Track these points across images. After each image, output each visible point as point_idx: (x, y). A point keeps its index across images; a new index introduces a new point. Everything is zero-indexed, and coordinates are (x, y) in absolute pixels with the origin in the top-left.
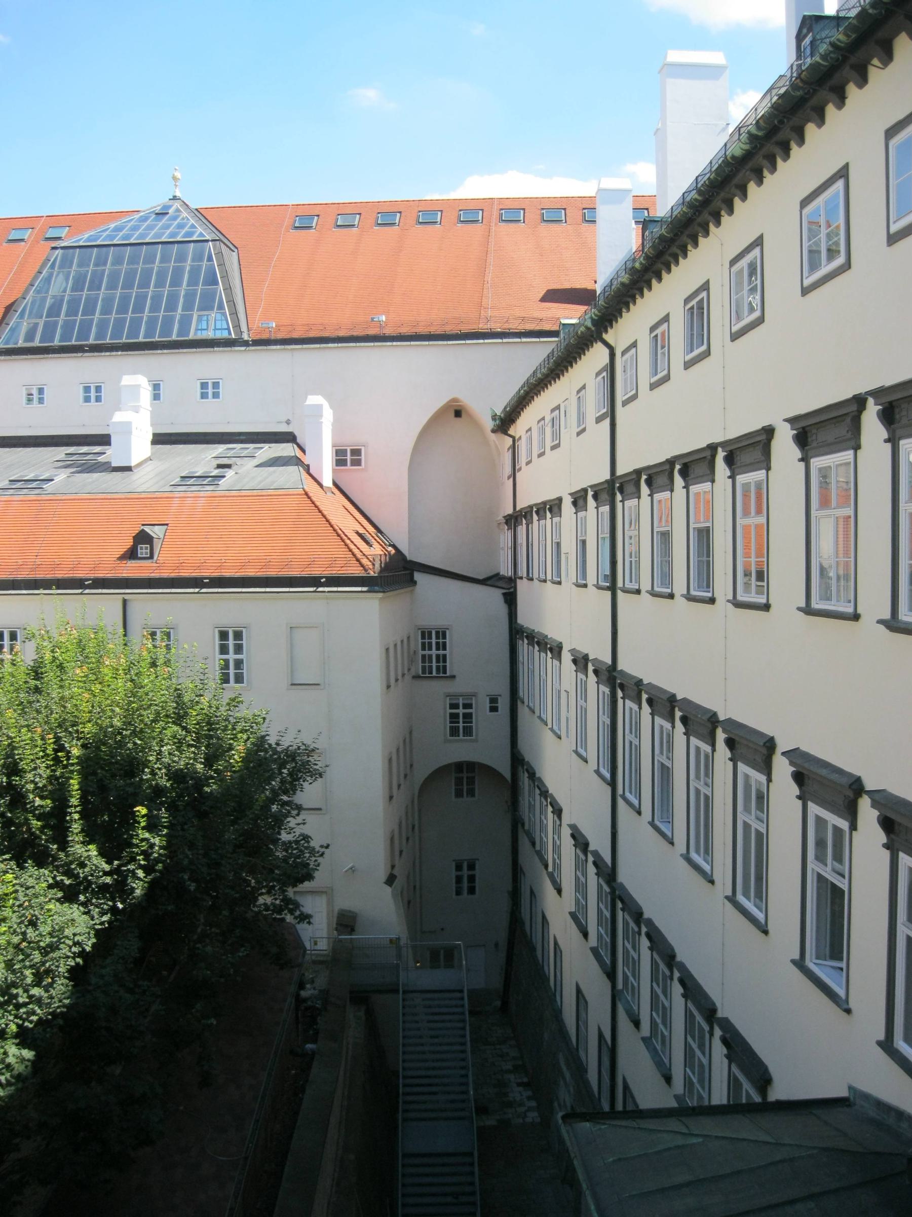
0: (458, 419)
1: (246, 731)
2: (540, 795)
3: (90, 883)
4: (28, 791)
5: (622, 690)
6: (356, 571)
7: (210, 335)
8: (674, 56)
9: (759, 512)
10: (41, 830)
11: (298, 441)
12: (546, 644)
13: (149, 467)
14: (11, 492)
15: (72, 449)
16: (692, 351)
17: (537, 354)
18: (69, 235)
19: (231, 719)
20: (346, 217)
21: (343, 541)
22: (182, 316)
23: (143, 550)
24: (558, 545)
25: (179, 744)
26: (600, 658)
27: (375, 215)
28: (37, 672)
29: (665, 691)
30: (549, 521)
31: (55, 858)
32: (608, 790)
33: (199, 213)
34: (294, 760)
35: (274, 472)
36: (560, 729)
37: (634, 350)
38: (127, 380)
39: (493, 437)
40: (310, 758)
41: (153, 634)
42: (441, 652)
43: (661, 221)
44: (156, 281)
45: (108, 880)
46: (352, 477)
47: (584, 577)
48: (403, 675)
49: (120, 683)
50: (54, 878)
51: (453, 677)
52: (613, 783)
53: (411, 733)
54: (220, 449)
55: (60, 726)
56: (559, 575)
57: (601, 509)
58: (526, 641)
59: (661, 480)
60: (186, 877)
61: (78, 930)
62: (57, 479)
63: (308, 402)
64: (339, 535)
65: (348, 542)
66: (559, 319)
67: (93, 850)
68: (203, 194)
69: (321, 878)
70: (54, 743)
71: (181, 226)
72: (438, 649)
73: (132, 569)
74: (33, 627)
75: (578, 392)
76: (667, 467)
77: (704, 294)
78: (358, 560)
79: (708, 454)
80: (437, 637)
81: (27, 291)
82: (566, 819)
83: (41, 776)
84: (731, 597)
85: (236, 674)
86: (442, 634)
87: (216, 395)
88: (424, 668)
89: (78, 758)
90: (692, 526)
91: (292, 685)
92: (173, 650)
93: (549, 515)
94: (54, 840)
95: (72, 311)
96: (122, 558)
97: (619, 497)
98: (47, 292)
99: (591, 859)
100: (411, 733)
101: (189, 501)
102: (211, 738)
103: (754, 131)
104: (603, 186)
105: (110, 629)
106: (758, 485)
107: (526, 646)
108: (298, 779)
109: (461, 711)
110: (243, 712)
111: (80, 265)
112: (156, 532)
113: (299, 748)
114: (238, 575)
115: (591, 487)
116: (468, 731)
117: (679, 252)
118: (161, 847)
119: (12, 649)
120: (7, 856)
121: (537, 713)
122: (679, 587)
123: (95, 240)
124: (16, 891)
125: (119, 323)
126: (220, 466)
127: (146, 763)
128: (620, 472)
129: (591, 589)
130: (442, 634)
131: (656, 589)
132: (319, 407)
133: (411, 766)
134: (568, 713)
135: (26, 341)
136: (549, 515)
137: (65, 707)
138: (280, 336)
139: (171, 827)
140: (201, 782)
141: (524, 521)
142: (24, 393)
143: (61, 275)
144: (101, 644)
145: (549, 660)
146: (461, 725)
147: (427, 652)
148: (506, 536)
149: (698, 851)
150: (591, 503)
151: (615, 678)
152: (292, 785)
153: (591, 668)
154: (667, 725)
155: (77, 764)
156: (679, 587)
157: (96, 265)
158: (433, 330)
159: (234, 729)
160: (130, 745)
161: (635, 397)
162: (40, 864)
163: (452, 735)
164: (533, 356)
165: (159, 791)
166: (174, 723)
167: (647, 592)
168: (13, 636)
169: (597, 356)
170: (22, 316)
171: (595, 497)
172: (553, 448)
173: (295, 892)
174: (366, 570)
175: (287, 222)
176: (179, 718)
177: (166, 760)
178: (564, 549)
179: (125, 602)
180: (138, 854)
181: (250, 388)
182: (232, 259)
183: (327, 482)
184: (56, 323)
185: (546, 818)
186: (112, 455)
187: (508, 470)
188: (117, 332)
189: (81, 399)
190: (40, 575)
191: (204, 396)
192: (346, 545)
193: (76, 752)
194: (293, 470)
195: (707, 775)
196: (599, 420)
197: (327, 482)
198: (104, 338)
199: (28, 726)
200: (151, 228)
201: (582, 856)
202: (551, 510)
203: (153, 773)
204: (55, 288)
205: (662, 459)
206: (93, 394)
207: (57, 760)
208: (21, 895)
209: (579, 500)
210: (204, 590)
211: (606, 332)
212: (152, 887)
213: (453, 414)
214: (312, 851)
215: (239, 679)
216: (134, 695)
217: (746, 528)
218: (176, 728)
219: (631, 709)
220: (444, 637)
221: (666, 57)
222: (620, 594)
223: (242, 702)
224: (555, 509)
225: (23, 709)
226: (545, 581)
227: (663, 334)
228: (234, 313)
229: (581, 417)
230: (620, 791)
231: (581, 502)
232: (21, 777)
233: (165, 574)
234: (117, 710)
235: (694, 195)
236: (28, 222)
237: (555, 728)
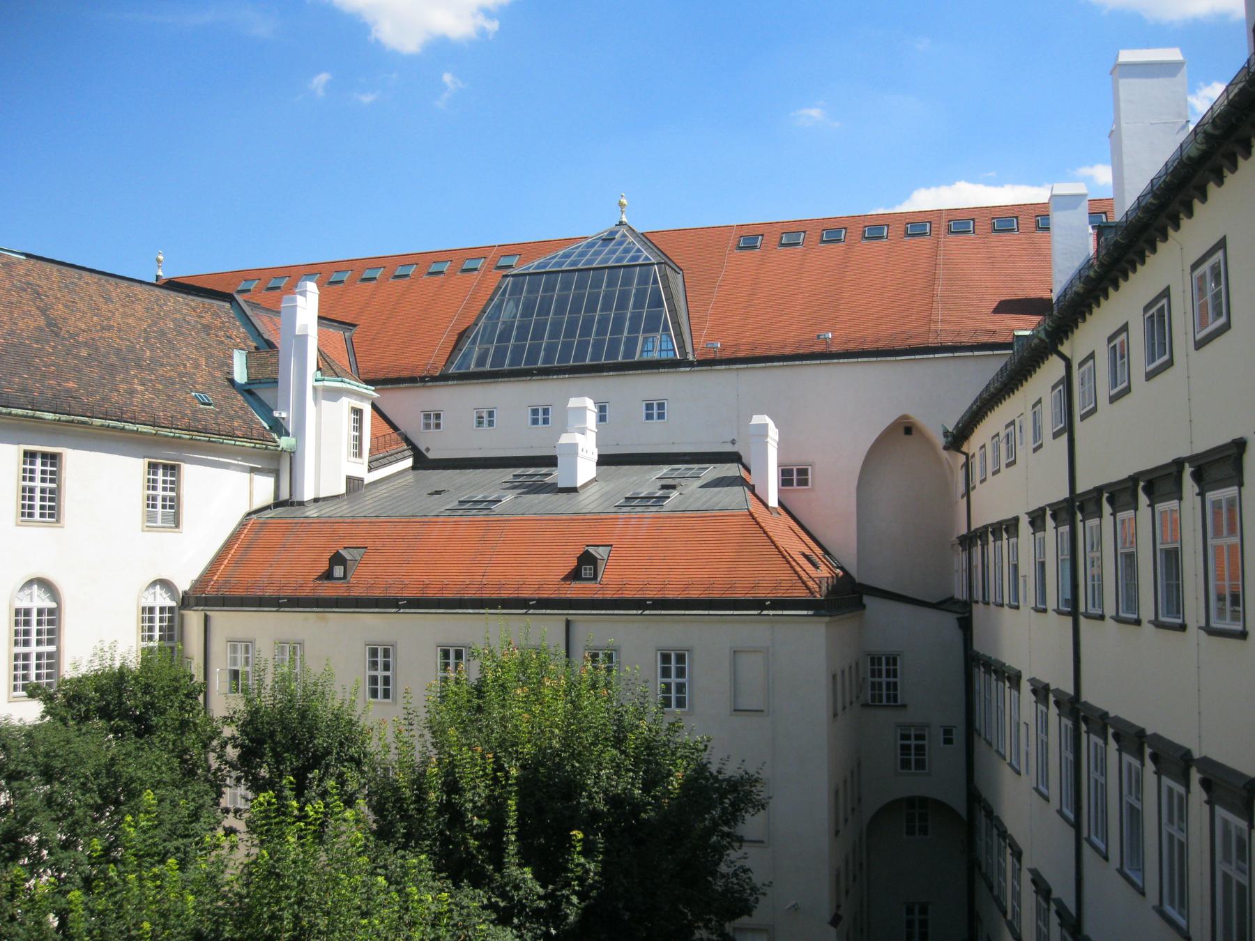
0: (908, 437)
2: (999, 835)
3: (524, 906)
4: (466, 810)
5: (1087, 724)
6: (801, 594)
7: (655, 356)
8: (1126, 56)
9: (1232, 531)
10: (479, 848)
12: (1004, 672)
13: (594, 488)
14: (461, 512)
15: (519, 471)
16: (1153, 361)
17: (987, 369)
20: (791, 235)
23: (587, 571)
24: (1016, 567)
25: (618, 768)
26: (1062, 688)
27: (819, 232)
28: (479, 690)
29: (1132, 726)
30: (1005, 542)
31: (492, 880)
32: (1072, 832)
33: (645, 238)
36: (1019, 763)
37: (1091, 362)
39: (945, 454)
41: (594, 657)
42: (892, 680)
43: (1116, 226)
44: (603, 304)
45: (542, 904)
46: (798, 496)
47: (1044, 600)
48: (851, 703)
49: (560, 704)
50: (489, 899)
51: (904, 706)
52: (1077, 825)
53: (859, 764)
54: (665, 469)
55: (500, 746)
56: (1017, 599)
57: (1061, 529)
58: (982, 669)
59: (1125, 498)
60: (620, 905)
62: (505, 500)
67: (528, 873)
68: (651, 217)
69: (760, 915)
71: (627, 251)
72: (888, 676)
73: (576, 590)
74: (479, 646)
75: (1034, 406)
76: (1130, 484)
77: (1164, 301)
78: (804, 582)
79: (1174, 469)
82: (1027, 862)
83: (480, 796)
84: (1203, 623)
86: (892, 660)
88: (873, 696)
89: (516, 778)
90: (1159, 546)
93: (1005, 536)
94: (489, 860)
95: (522, 336)
96: (566, 579)
97: (1079, 516)
99: (1053, 907)
100: (859, 764)
102: (650, 762)
103: (1209, 128)
104: (1055, 192)
105: (552, 650)
106: (1231, 503)
108: (740, 810)
109: (913, 742)
110: (684, 737)
112: (600, 553)
115: (1049, 505)
116: (920, 765)
117: (1135, 258)
118: (595, 874)
119: (457, 665)
120: (444, 875)
121: (995, 747)
122: (1147, 612)
123: (545, 267)
124: (451, 911)
125: (567, 346)
126: (664, 487)
127: (583, 787)
128: (1080, 489)
129: (1051, 615)
131: (1121, 614)
132: (765, 427)
133: (860, 800)
134: (1028, 745)
136: (1005, 536)
137: (506, 727)
138: (726, 355)
139: (606, 852)
140: (638, 807)
142: (475, 415)
144: (543, 665)
145: (1007, 691)
146: (913, 757)
147: (877, 679)
148: (960, 559)
149: (1172, 904)
150: (1050, 523)
151: (1078, 711)
152: (733, 815)
153: (1052, 699)
154: (1136, 763)
155: (516, 784)
156: (1147, 612)
157: (545, 291)
160: (568, 768)
161: (1094, 410)
162: (476, 885)
163: (903, 767)
164: (980, 373)
165: (595, 815)
166: (613, 746)
167: (1112, 617)
168: (459, 655)
169: (1052, 369)
170: (474, 342)
171: (1054, 516)
172: (1008, 465)
173: (734, 929)
175: (732, 242)
176: (619, 742)
177: (603, 784)
178: (1021, 572)
179: (568, 623)
180: (572, 879)
181: (694, 409)
182: (677, 281)
183: (773, 502)
185: (1005, 861)
186: (558, 476)
187: (961, 488)
188: (565, 356)
189: (529, 421)
190: (486, 594)
193: (514, 772)
194: (738, 490)
195: (1181, 818)
196: (1056, 435)
197: (773, 502)
198: (483, 365)
199: (469, 745)
200: (597, 253)
201: (1044, 905)
203: (590, 797)
204: (505, 316)
205: (1125, 475)
206: (540, 417)
207: (496, 780)
208: (455, 914)
209: (1037, 520)
210: (647, 612)
211: (1062, 343)
212: (585, 914)
214: (754, 889)
215: (681, 703)
217: (1218, 549)
218: (615, 752)
219: (1096, 745)
220: (895, 663)
221: (1117, 57)
222: (1082, 619)
224: (1012, 529)
226: (1002, 605)
227: (1122, 343)
228: (679, 335)
229: (1037, 433)
230: (1085, 834)
231: (1039, 522)
232: (461, 795)
233: (609, 594)
234: (557, 731)
235: (1149, 199)
237: (1014, 763)
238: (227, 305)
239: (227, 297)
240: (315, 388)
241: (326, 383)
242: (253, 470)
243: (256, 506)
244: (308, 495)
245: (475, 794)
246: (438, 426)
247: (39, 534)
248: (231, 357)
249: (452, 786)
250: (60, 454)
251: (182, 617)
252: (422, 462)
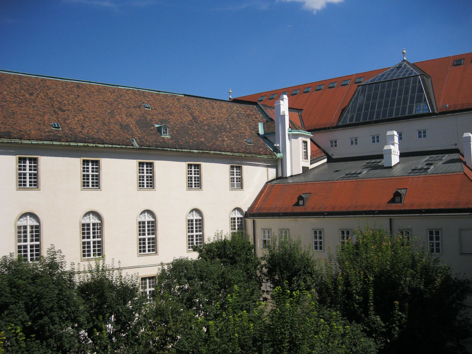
1: (441, 273)
3: (377, 331)
10: (359, 308)
13: (399, 166)
14: (346, 178)
15: (368, 161)
19: (435, 267)
22: (410, 106)
23: (397, 199)
25: (413, 277)
28: (357, 246)
31: (364, 320)
33: (414, 65)
35: (450, 166)
40: (470, 286)
41: (402, 233)
45: (384, 330)
50: (363, 328)
54: (427, 157)
55: (366, 268)
61: (372, 350)
71: (407, 71)
73: (393, 207)
81: (349, 103)
83: (359, 288)
85: (436, 249)
87: (425, 136)
89: (373, 281)
91: (461, 254)
95: (367, 109)
102: (427, 273)
110: (440, 265)
112: (402, 192)
113: (465, 281)
120: (345, 318)
126: (427, 164)
127: (400, 284)
135: (349, 121)
137: (367, 261)
144: (381, 237)
159: (436, 272)
160: (393, 277)
162: (358, 322)
166: (411, 268)
168: (348, 233)
179: (391, 220)
182: (429, 81)
186: (384, 162)
188: (384, 115)
190: (358, 210)
191: (420, 137)
198: (352, 121)
200: (395, 73)
203: (403, 289)
206: (376, 139)
207: (365, 282)
210: (423, 215)
215: (438, 251)
216: (395, 257)
218: (412, 271)
223: (439, 261)
225: (352, 261)
233: (407, 208)
238: (255, 106)
239: (255, 104)
240: (289, 134)
241: (293, 132)
242: (268, 166)
245: (357, 287)
246: (336, 146)
247: (195, 193)
248: (258, 125)
249: (347, 284)
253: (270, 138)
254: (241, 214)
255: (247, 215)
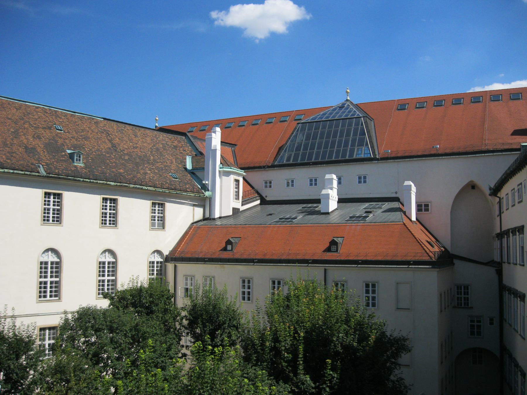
1: (376, 329)
4: (282, 350)
6: (427, 258)
7: (362, 156)
10: (287, 367)
11: (401, 200)
12: (517, 294)
13: (337, 213)
15: (304, 205)
18: (304, 118)
21: (421, 245)
23: (333, 248)
25: (347, 334)
28: (288, 298)
30: (518, 236)
31: (292, 379)
33: (357, 106)
34: (398, 343)
38: (328, 176)
41: (337, 285)
45: (314, 390)
46: (424, 215)
48: (448, 306)
50: (291, 389)
51: (472, 308)
54: (367, 205)
55: (297, 323)
58: (507, 292)
62: (299, 218)
63: (405, 184)
64: (419, 242)
65: (423, 245)
66: (520, 143)
70: (294, 330)
71: (350, 112)
73: (328, 256)
78: (427, 254)
80: (464, 289)
83: (288, 344)
86: (466, 287)
91: (398, 308)
92: (345, 292)
93: (517, 234)
95: (305, 148)
98: (296, 141)
101: (353, 227)
102: (361, 330)
105: (319, 282)
107: (507, 295)
109: (476, 324)
110: (375, 320)
111: (309, 130)
112: (339, 240)
114: (374, 259)
116: (479, 333)
118: (337, 378)
119: (278, 288)
125: (325, 153)
126: (366, 212)
130: (466, 287)
136: (517, 234)
138: (392, 156)
141: (506, 236)
142: (286, 182)
143: (301, 135)
145: (519, 302)
147: (460, 296)
148: (497, 243)
152: (396, 355)
157: (315, 129)
158: (461, 150)
159: (371, 328)
162: (285, 382)
165: (337, 353)
166: (345, 324)
168: (279, 283)
170: (285, 151)
172: (519, 202)
174: (431, 258)
179: (325, 270)
181: (379, 179)
182: (371, 124)
183: (414, 218)
184: (299, 153)
186: (321, 207)
187: (497, 213)
188: (324, 157)
190: (291, 258)
191: (360, 182)
192: (422, 247)
193: (302, 334)
194: (398, 213)
197: (414, 218)
200: (337, 113)
202: (518, 231)
203: (335, 346)
204: (298, 140)
206: (313, 182)
207: (294, 338)
210: (359, 266)
213: (471, 187)
214: (406, 387)
215: (374, 305)
216: (328, 311)
218: (345, 326)
220: (468, 289)
226: (516, 264)
228: (372, 147)
233: (343, 258)
234: (321, 317)
236: (288, 114)
237: (522, 334)
238: (184, 138)
239: (184, 134)
240: (219, 171)
241: (224, 169)
242: (194, 205)
243: (196, 220)
244: (217, 215)
246: (270, 187)
248: (186, 159)
250: (117, 199)
251: (166, 266)
252: (264, 202)
253: (199, 174)
254: (162, 258)
255: (168, 259)
